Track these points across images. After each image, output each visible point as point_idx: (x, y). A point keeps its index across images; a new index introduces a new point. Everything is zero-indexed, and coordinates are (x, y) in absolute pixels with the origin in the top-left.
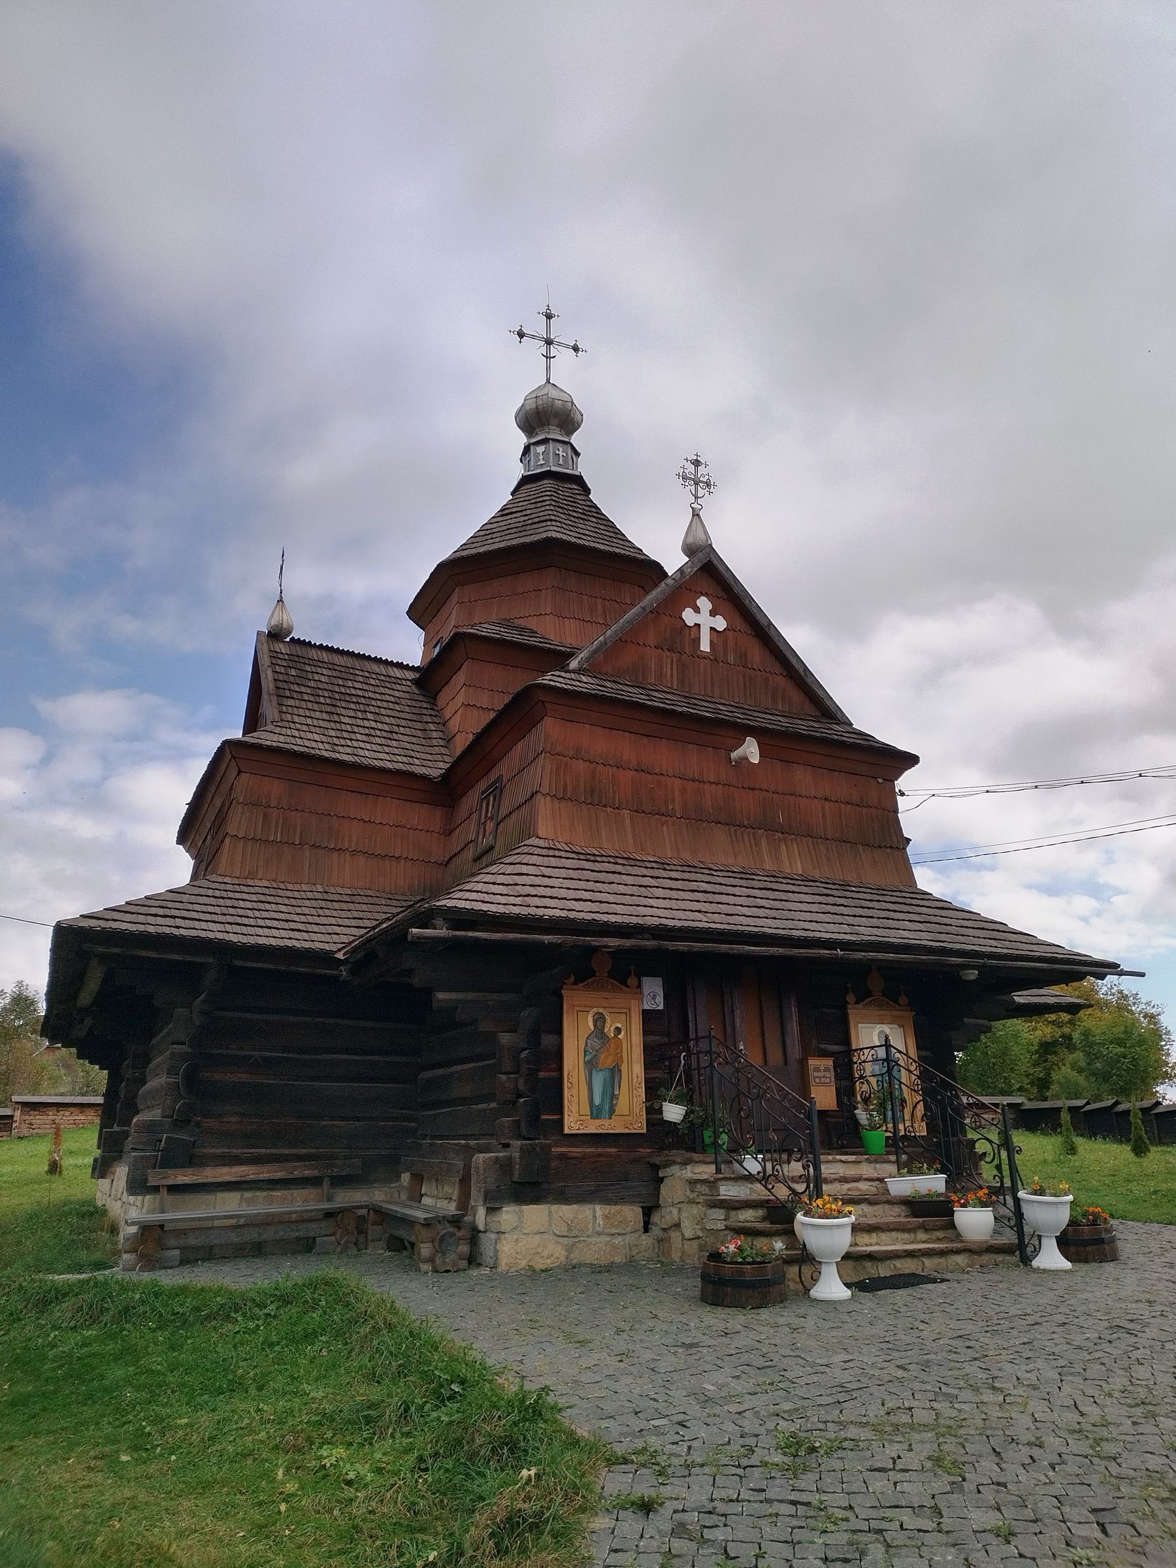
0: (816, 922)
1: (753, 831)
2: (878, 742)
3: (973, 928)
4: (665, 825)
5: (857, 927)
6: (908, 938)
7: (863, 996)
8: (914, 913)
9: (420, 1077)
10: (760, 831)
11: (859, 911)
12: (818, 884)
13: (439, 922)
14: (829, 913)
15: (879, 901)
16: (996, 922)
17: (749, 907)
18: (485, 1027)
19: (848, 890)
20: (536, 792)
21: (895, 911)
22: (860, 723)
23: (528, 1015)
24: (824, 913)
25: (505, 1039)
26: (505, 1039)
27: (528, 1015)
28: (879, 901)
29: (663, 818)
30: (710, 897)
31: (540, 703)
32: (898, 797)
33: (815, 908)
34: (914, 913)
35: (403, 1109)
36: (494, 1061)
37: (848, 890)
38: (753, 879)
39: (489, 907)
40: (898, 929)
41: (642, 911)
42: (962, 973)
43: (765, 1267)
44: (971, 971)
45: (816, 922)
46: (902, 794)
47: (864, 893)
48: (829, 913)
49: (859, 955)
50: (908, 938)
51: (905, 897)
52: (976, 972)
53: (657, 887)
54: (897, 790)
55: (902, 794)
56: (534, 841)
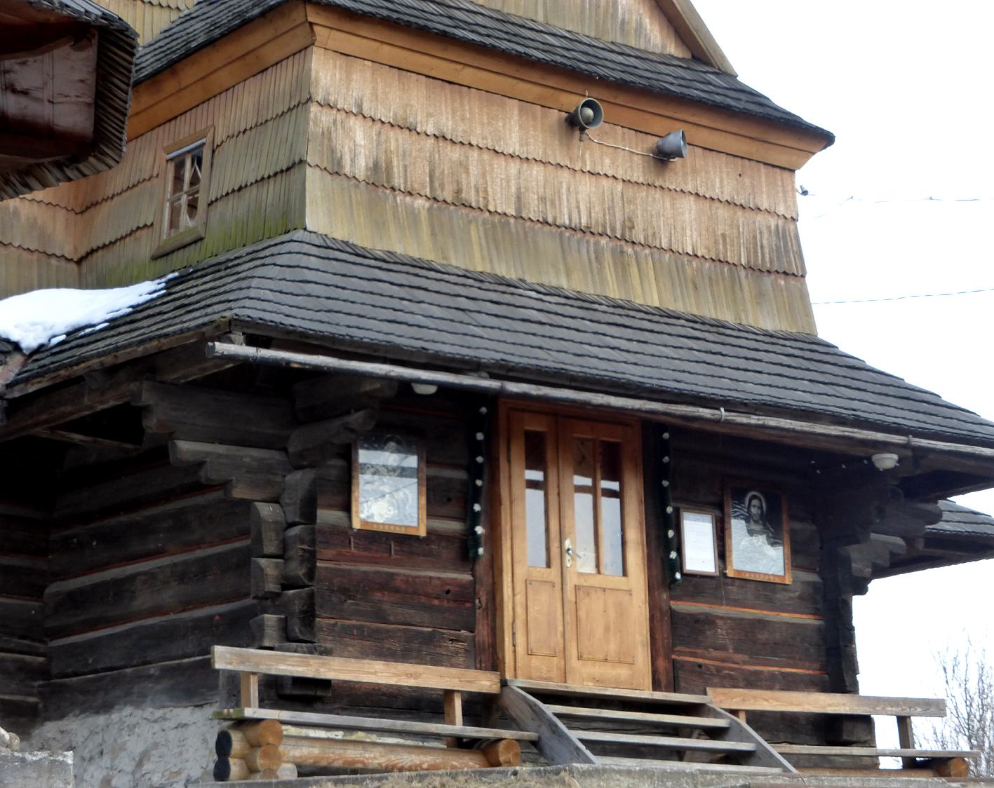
0: (689, 373)
1: (592, 240)
2: (777, 109)
3: (895, 397)
4: (473, 223)
5: (742, 383)
6: (810, 402)
7: (679, 564)
8: (816, 371)
9: (47, 591)
10: (604, 241)
11: (742, 363)
12: (682, 322)
13: (237, 336)
14: (704, 362)
15: (767, 351)
16: (926, 392)
17: (599, 346)
18: (239, 493)
19: (723, 334)
20: (301, 161)
21: (789, 366)
22: (748, 75)
23: (299, 480)
24: (697, 362)
25: (267, 511)
26: (267, 511)
27: (299, 480)
28: (767, 351)
29: (473, 214)
30: (547, 330)
31: (307, 24)
32: (799, 197)
33: (683, 354)
34: (816, 371)
35: (23, 637)
36: (249, 542)
37: (723, 334)
38: (595, 310)
39: (328, 317)
40: (796, 390)
41: (477, 342)
42: (875, 458)
43: (656, 686)
44: (889, 455)
45: (689, 373)
46: (805, 193)
47: (747, 339)
48: (704, 362)
49: (754, 420)
50: (810, 402)
51: (801, 349)
52: (895, 457)
53: (479, 312)
54: (797, 186)
55: (805, 193)
56: (299, 235)
